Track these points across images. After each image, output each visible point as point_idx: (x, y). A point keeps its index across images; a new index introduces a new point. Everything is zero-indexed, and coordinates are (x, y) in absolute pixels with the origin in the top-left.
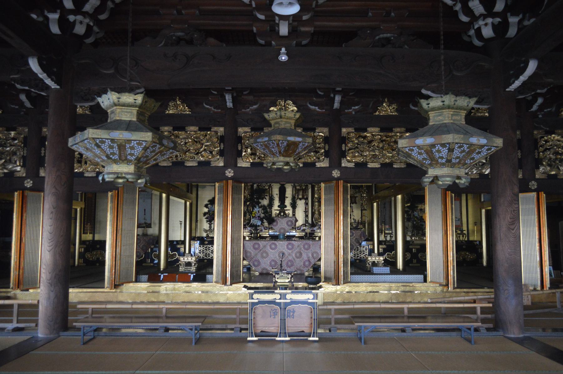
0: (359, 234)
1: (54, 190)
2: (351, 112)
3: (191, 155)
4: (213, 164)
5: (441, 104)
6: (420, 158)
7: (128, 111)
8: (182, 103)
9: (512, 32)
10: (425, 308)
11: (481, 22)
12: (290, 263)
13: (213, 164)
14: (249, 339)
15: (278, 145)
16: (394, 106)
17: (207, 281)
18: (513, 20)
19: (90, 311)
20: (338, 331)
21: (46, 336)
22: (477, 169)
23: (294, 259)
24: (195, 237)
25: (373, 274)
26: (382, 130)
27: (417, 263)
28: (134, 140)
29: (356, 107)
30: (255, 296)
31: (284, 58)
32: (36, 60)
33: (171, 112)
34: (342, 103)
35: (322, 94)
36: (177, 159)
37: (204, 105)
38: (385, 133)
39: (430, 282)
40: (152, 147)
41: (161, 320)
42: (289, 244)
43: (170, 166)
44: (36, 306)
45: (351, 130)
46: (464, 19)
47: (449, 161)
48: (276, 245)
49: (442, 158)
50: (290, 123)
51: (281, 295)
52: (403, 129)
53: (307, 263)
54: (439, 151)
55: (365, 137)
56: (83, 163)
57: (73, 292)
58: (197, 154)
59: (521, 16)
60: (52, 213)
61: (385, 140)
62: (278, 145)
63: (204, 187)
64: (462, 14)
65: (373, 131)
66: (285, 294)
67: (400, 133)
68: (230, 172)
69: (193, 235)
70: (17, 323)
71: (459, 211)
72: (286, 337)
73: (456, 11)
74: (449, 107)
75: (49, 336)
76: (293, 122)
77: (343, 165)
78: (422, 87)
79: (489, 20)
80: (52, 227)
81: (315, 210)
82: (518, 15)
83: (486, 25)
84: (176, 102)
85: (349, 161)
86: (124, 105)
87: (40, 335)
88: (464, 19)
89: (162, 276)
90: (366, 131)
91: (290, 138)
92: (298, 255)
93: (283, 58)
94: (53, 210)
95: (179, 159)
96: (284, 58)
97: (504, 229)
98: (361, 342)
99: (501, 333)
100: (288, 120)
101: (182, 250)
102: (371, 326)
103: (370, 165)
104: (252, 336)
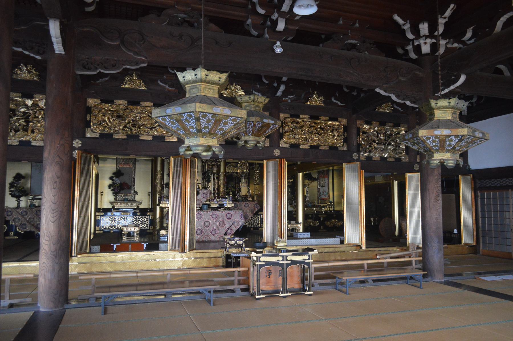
0: (253, 205)
1: (57, 159)
3: (146, 129)
5: (194, 77)
6: (432, 144)
7: (211, 87)
8: (138, 78)
9: (442, 50)
10: (229, 272)
11: (422, 41)
12: (214, 232)
14: (257, 297)
15: (254, 125)
16: (322, 98)
17: (160, 249)
18: (442, 42)
19: (366, 266)
20: (173, 296)
21: (50, 310)
22: (379, 153)
23: (218, 228)
24: (100, 209)
25: (297, 238)
26: (312, 117)
27: (324, 229)
28: (232, 117)
29: (292, 97)
30: (262, 259)
31: (279, 50)
32: (58, 23)
33: (127, 86)
34: (283, 92)
35: (267, 82)
36: (132, 133)
37: (159, 82)
38: (313, 121)
41: (166, 286)
42: (214, 214)
44: (35, 279)
45: (287, 115)
46: (410, 36)
47: (454, 148)
48: (202, 215)
49: (450, 145)
50: (259, 107)
51: (283, 257)
52: (327, 118)
55: (298, 123)
56: (30, 131)
57: (72, 265)
58: (151, 129)
59: (448, 40)
60: (56, 182)
61: (313, 126)
62: (254, 125)
63: (105, 160)
64: (410, 32)
65: (304, 117)
66: (287, 256)
67: (325, 121)
69: (99, 207)
70: (10, 299)
72: (287, 293)
73: (404, 30)
75: (54, 310)
76: (262, 106)
77: (281, 145)
78: (377, 87)
79: (429, 41)
81: (221, 184)
82: (446, 39)
83: (425, 43)
84: (133, 77)
85: (285, 143)
86: (209, 82)
87: (41, 309)
88: (410, 36)
89: (115, 246)
90: (298, 117)
91: (265, 120)
92: (221, 224)
93: (278, 51)
94: (57, 180)
95: (134, 132)
96: (279, 50)
97: (433, 200)
98: (210, 304)
99: (430, 279)
100: (258, 104)
102: (353, 279)
103: (302, 147)
104: (260, 295)
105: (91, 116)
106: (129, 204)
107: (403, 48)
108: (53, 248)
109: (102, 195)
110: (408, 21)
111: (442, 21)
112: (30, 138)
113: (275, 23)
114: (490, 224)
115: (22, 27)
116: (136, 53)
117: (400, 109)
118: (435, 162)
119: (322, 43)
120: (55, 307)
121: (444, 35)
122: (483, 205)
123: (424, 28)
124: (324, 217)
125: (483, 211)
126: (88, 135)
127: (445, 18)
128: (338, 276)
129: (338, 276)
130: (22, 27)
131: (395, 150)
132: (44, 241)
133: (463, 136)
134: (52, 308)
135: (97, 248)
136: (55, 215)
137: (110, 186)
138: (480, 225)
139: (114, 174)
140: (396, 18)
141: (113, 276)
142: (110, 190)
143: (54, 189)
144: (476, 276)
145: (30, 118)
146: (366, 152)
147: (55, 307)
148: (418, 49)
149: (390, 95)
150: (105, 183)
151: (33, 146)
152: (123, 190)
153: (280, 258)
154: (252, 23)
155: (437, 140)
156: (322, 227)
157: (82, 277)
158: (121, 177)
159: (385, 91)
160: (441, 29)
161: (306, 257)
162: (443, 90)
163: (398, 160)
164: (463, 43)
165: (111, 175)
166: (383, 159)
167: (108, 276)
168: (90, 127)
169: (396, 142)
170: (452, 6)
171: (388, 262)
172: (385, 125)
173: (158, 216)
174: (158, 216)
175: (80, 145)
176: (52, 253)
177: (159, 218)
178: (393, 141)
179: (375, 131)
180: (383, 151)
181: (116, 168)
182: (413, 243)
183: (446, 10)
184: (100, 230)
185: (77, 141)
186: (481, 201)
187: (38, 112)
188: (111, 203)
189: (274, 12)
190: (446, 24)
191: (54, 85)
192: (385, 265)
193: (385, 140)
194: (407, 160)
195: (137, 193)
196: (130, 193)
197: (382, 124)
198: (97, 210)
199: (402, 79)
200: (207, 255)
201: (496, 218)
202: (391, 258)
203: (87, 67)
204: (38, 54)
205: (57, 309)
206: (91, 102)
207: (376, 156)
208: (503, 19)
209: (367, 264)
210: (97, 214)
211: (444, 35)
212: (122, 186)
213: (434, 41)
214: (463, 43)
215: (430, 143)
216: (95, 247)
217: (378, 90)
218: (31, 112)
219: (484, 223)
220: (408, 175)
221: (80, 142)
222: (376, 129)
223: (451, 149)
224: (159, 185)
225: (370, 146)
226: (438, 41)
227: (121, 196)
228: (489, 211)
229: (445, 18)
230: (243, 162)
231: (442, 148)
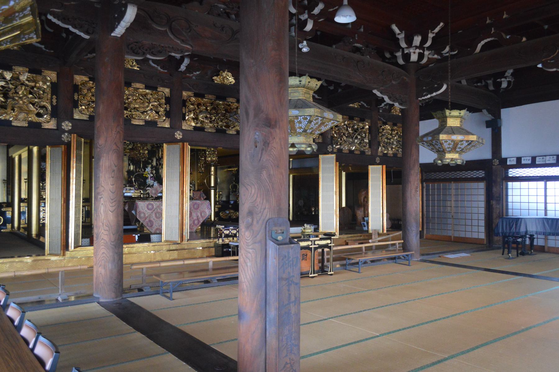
1: (114, 147)
2: (191, 78)
3: (137, 113)
4: (160, 125)
5: (298, 83)
9: (425, 60)
11: (412, 50)
13: (160, 125)
18: (426, 53)
21: (112, 300)
29: (198, 73)
31: (305, 50)
39: (48, 255)
40: (315, 120)
41: (209, 273)
43: (143, 125)
45: (190, 93)
46: (403, 45)
47: (305, 131)
49: (301, 128)
53: (196, 222)
54: (300, 122)
60: (114, 171)
66: (315, 241)
68: (179, 135)
71: (88, 175)
73: (398, 39)
74: (304, 87)
78: (375, 89)
80: (114, 186)
88: (403, 45)
94: (115, 168)
97: (413, 191)
101: (9, 215)
105: (78, 96)
107: (392, 54)
108: (113, 238)
110: (403, 32)
111: (431, 35)
112: (11, 117)
113: (305, 23)
114: (433, 212)
115: (72, 3)
116: (183, 41)
117: (365, 105)
118: (448, 160)
119: (335, 44)
120: (116, 297)
121: (429, 48)
122: (428, 195)
123: (417, 40)
125: (428, 200)
126: (76, 116)
127: (433, 33)
128: (352, 257)
129: (352, 257)
130: (72, 3)
131: (360, 143)
132: (103, 231)
133: (472, 141)
134: (113, 298)
136: (114, 204)
138: (425, 213)
140: (395, 28)
141: (163, 264)
143: (113, 177)
144: (440, 255)
145: (10, 94)
146: (337, 145)
147: (116, 297)
148: (407, 57)
149: (384, 96)
151: (14, 126)
153: (309, 243)
154: (467, 81)
155: (452, 143)
157: (134, 267)
159: (381, 93)
160: (429, 44)
161: (329, 241)
162: (427, 95)
163: (363, 153)
164: (441, 55)
166: (351, 152)
167: (158, 265)
168: (78, 108)
169: (362, 137)
170: (442, 24)
171: (376, 246)
172: (353, 119)
175: (70, 128)
176: (112, 243)
178: (359, 134)
179: (345, 125)
180: (353, 143)
182: (375, 230)
183: (437, 27)
185: (67, 122)
186: (426, 192)
187: (19, 87)
189: (304, 13)
190: (433, 38)
191: (109, 69)
192: (374, 248)
193: (353, 133)
194: (370, 153)
197: (351, 118)
199: (394, 82)
201: (439, 206)
202: (379, 241)
203: (136, 51)
204: (87, 33)
205: (118, 299)
206: (79, 79)
207: (345, 148)
208: (483, 43)
209: (365, 247)
211: (429, 48)
213: (421, 51)
214: (441, 55)
215: (446, 146)
217: (375, 91)
218: (11, 86)
219: (428, 211)
220: (370, 167)
221: (71, 125)
222: (346, 123)
223: (303, 131)
225: (341, 139)
226: (424, 51)
228: (433, 200)
229: (433, 33)
230: (212, 149)
231: (454, 149)
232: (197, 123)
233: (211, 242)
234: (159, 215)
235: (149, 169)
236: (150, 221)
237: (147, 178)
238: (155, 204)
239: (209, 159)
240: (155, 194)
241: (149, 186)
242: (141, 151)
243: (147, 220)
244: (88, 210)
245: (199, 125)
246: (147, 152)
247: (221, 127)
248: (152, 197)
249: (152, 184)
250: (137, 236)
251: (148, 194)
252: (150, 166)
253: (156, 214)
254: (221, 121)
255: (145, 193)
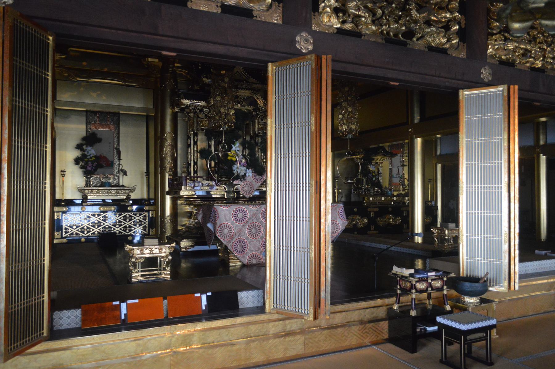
24: (60, 201)
69: (58, 197)
106: (113, 191)
109: (63, 176)
124: (375, 212)
135: (70, 318)
137: (77, 161)
139: (84, 139)
142: (77, 167)
150: (68, 156)
152: (101, 167)
156: (372, 228)
158: (98, 146)
165: (78, 141)
173: (168, 212)
174: (168, 212)
177: (171, 215)
181: (87, 131)
184: (62, 238)
188: (81, 190)
195: (125, 173)
196: (112, 174)
198: (56, 202)
200: (355, 316)
210: (56, 209)
212: (96, 163)
216: (66, 314)
224: (169, 159)
227: (95, 179)
232: (344, 22)
233: (377, 307)
234: (259, 231)
235: (237, 147)
236: (240, 241)
237: (233, 163)
238: (250, 210)
239: (344, 127)
240: (249, 192)
241: (238, 177)
242: (222, 110)
243: (234, 240)
244: (152, 217)
245: (348, 26)
246: (233, 112)
247: (396, 35)
248: (244, 197)
249: (242, 174)
250: (204, 297)
251: (238, 192)
252: (241, 140)
253: (250, 229)
254: (397, 22)
255: (231, 190)
